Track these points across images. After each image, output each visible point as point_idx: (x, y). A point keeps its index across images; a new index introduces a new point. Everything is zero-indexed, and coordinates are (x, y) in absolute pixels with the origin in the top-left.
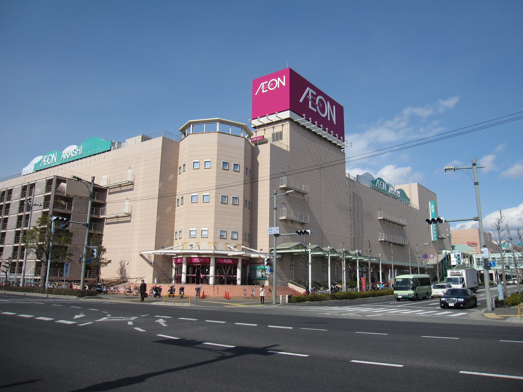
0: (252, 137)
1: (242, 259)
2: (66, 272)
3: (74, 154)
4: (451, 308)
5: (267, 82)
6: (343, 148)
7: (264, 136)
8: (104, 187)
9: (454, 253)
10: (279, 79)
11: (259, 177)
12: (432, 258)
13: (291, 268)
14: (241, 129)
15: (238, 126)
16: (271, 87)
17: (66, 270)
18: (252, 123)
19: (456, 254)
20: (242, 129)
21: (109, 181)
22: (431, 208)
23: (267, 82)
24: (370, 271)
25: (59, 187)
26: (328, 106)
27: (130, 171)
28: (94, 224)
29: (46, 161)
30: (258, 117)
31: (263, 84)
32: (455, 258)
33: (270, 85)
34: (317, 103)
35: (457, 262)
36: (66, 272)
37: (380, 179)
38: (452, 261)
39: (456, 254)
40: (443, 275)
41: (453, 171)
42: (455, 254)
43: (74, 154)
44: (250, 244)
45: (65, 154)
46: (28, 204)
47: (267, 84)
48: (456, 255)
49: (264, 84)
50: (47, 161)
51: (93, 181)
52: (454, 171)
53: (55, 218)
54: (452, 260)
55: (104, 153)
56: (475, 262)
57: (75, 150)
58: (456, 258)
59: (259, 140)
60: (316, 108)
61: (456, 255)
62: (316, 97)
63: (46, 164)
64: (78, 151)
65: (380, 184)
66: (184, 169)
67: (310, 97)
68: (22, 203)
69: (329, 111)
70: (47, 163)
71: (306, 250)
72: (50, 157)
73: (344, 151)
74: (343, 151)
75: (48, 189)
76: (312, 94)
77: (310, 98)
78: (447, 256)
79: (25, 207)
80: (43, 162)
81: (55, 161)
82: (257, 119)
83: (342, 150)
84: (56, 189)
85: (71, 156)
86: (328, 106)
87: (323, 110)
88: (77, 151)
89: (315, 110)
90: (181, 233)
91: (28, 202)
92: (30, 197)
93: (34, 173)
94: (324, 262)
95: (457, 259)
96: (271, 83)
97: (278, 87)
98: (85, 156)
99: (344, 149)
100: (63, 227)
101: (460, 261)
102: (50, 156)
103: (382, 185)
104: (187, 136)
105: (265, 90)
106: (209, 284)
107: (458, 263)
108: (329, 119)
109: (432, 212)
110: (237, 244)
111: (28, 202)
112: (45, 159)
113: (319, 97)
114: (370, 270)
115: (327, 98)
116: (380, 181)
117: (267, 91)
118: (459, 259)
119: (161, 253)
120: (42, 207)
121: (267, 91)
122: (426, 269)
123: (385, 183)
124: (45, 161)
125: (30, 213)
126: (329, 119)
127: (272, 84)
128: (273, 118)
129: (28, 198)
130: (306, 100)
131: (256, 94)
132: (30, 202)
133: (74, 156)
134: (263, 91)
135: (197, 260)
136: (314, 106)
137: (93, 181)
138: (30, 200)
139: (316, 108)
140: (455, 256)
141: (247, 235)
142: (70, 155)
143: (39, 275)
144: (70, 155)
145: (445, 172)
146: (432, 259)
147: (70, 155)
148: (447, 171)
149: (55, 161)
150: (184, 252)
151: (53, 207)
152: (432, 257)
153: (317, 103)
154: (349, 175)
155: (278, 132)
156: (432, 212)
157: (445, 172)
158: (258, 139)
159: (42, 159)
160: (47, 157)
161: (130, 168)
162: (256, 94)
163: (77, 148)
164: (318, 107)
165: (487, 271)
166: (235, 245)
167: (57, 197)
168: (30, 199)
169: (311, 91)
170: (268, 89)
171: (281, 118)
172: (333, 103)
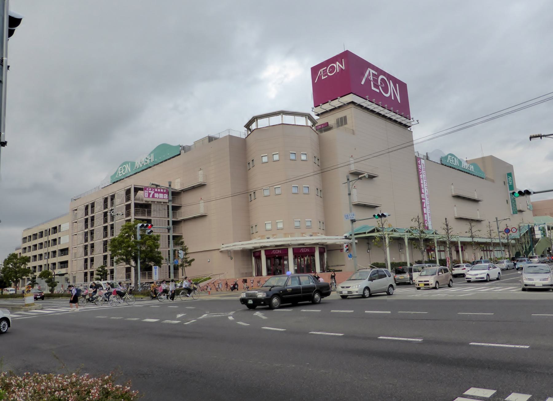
0: (316, 125)
1: (319, 247)
2: (156, 274)
3: (146, 163)
4: (551, 289)
5: (326, 68)
6: (410, 127)
7: (328, 123)
8: (179, 191)
9: (538, 226)
10: (338, 63)
11: (240, 137)
12: (515, 232)
13: (368, 252)
14: (305, 118)
15: (302, 116)
16: (330, 73)
17: (155, 272)
19: (540, 226)
20: (306, 117)
21: (182, 184)
22: (508, 180)
23: (326, 68)
25: (137, 195)
26: (391, 86)
27: (201, 172)
28: (148, 273)
29: (121, 172)
30: (320, 104)
31: (322, 70)
32: (540, 231)
33: (329, 70)
34: (379, 84)
35: (542, 235)
36: (156, 274)
37: (452, 155)
39: (540, 226)
40: (526, 249)
41: (539, 139)
43: (146, 163)
45: (138, 163)
46: (111, 214)
47: (326, 69)
49: (323, 70)
50: (122, 172)
51: (170, 185)
52: (541, 138)
53: (140, 225)
54: (536, 233)
55: (175, 158)
57: (147, 158)
58: (541, 231)
59: (324, 127)
60: (379, 89)
61: (540, 228)
62: (378, 76)
63: (121, 175)
64: (150, 159)
65: (451, 159)
66: (253, 164)
67: (371, 78)
68: (105, 214)
69: (392, 91)
70: (122, 174)
72: (124, 168)
73: (411, 129)
74: (410, 130)
75: (128, 199)
76: (373, 75)
77: (372, 79)
78: (531, 228)
79: (109, 218)
80: (119, 173)
81: (130, 171)
82: (319, 107)
83: (409, 129)
84: (134, 198)
85: (144, 165)
86: (391, 86)
87: (386, 90)
88: (149, 158)
89: (378, 91)
90: (257, 227)
91: (111, 212)
92: (113, 208)
93: (111, 184)
94: (400, 244)
95: (542, 232)
96: (330, 68)
97: (338, 71)
98: (169, 158)
99: (410, 128)
100: (149, 233)
101: (546, 233)
102: (124, 167)
103: (454, 161)
104: (252, 132)
105: (324, 76)
107: (543, 236)
108: (393, 98)
109: (510, 184)
110: (313, 233)
111: (111, 212)
112: (120, 170)
113: (381, 77)
115: (390, 77)
116: (451, 156)
117: (327, 77)
118: (544, 232)
119: (240, 248)
120: (124, 216)
121: (327, 77)
123: (457, 158)
124: (120, 172)
125: (114, 223)
126: (393, 98)
127: (331, 70)
128: (336, 103)
129: (111, 209)
130: (368, 81)
131: (316, 82)
132: (112, 212)
133: (146, 164)
134: (323, 78)
135: (275, 252)
136: (376, 86)
137: (170, 185)
138: (113, 211)
139: (379, 89)
140: (539, 228)
141: (321, 223)
142: (143, 164)
143: (129, 279)
144: (142, 163)
145: (530, 140)
146: (515, 233)
147: (143, 164)
148: (532, 139)
149: (130, 171)
150: (262, 246)
151: (135, 215)
152: (515, 232)
153: (379, 84)
154: (418, 153)
155: (342, 117)
156: (510, 184)
157: (530, 140)
158: (322, 126)
159: (117, 171)
160: (122, 168)
161: (200, 169)
162: (316, 82)
163: (148, 156)
164: (380, 87)
166: (311, 234)
167: (136, 205)
168: (112, 210)
169: (372, 71)
170: (327, 74)
171: (343, 103)
172: (396, 81)
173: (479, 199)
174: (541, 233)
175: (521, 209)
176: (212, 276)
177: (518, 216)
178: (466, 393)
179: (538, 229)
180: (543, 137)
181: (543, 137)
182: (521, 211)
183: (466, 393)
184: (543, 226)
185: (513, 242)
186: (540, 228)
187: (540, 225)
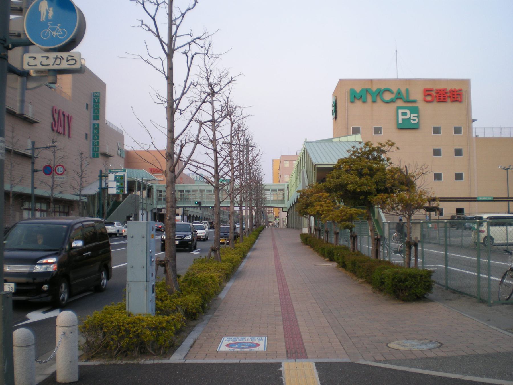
18: (238, 208)
19: (118, 174)
24: (117, 307)
32: (116, 182)
38: (509, 204)
42: (116, 174)
44: (309, 223)
48: (118, 176)
51: (59, 149)
56: (155, 196)
61: (117, 177)
71: (254, 207)
95: (119, 184)
106: (315, 363)
114: (89, 317)
122: (162, 242)
140: (115, 178)
146: (60, 176)
152: (60, 173)
165: (155, 17)
173: (35, 119)
174: (117, 186)
175: (107, 152)
176: (241, 120)
177: (100, 160)
178: (38, 262)
179: (113, 179)
180: (35, 186)
181: (35, 186)
182: (106, 156)
183: (38, 262)
184: (122, 174)
185: (85, 199)
186: (117, 177)
187: (118, 172)
